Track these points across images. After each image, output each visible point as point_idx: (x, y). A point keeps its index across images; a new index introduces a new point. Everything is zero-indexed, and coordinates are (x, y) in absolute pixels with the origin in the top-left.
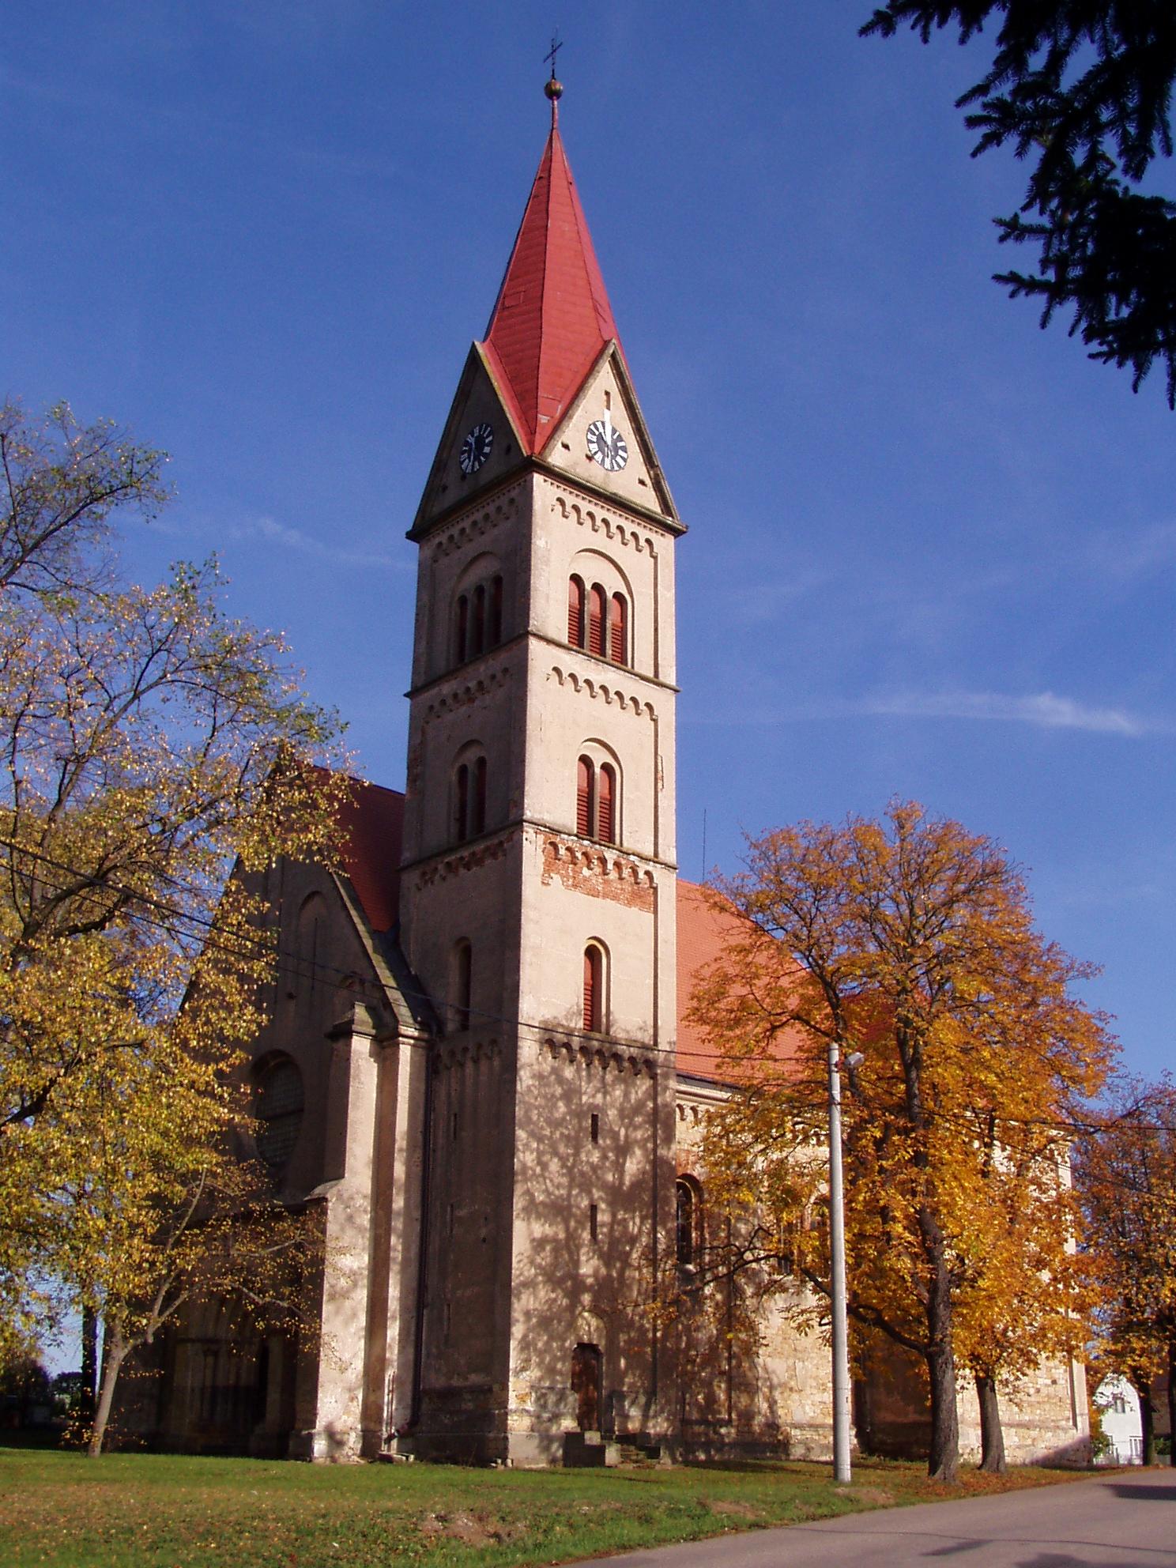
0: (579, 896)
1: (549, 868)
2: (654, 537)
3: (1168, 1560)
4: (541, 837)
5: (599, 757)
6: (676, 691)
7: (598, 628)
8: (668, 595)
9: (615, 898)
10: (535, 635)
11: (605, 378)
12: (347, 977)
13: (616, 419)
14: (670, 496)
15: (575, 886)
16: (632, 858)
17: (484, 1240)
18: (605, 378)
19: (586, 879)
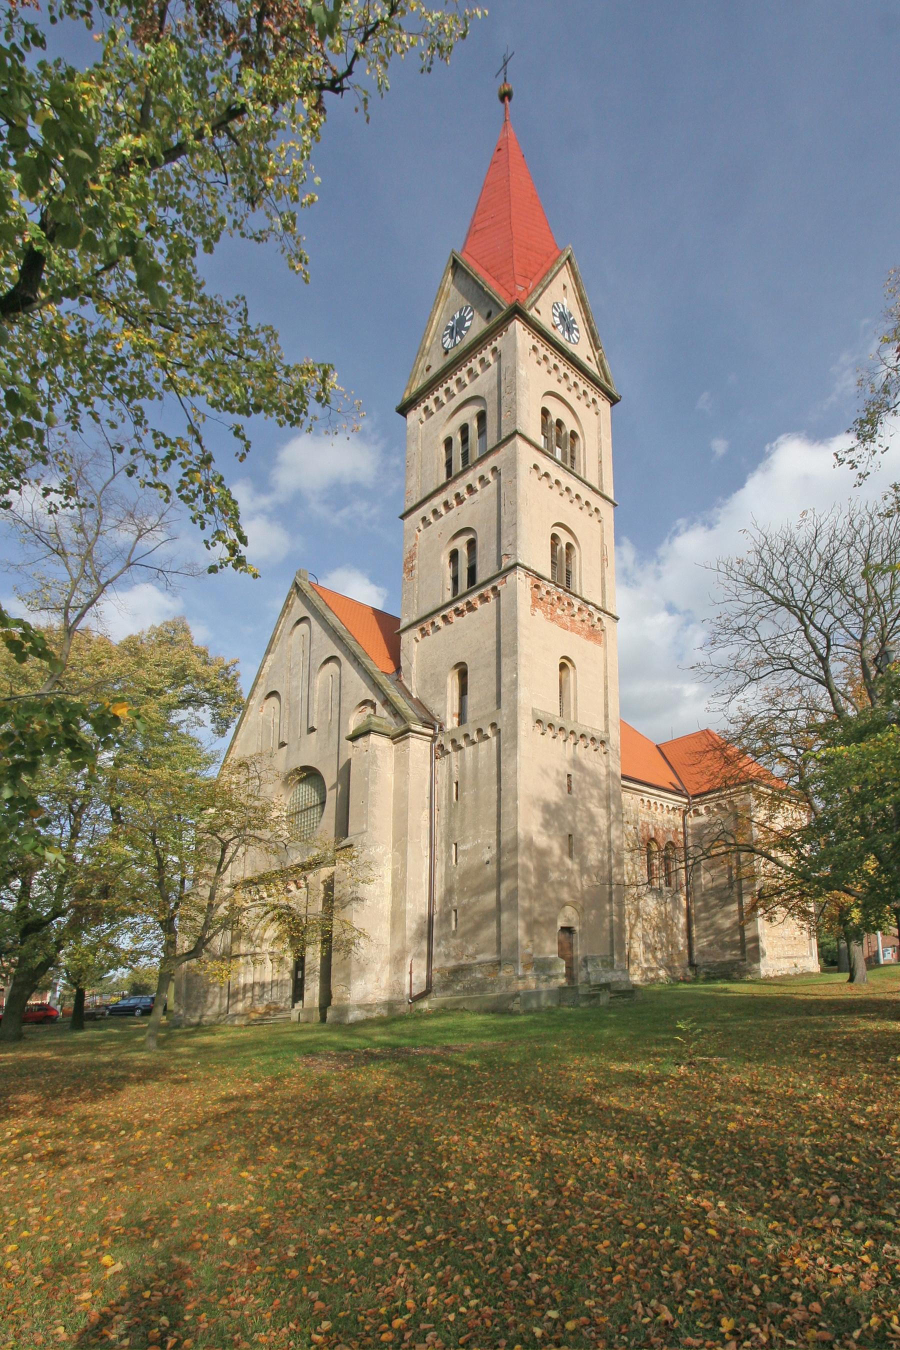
0: (554, 626)
1: (534, 605)
2: (598, 400)
3: (829, 1263)
4: (529, 580)
5: (565, 538)
6: (615, 505)
7: (560, 440)
8: (607, 442)
9: (578, 633)
10: (521, 435)
11: (564, 277)
12: (132, 393)
13: (570, 304)
14: (608, 371)
15: (552, 620)
16: (590, 607)
17: (488, 863)
18: (564, 277)
19: (559, 617)
